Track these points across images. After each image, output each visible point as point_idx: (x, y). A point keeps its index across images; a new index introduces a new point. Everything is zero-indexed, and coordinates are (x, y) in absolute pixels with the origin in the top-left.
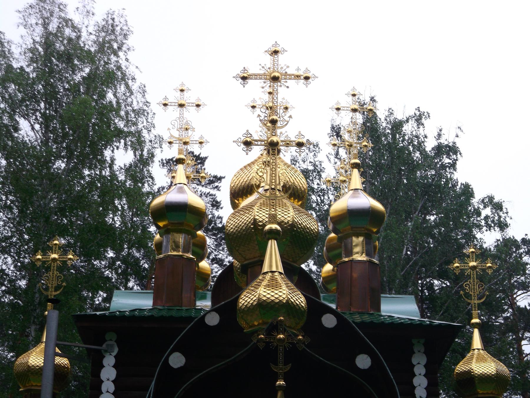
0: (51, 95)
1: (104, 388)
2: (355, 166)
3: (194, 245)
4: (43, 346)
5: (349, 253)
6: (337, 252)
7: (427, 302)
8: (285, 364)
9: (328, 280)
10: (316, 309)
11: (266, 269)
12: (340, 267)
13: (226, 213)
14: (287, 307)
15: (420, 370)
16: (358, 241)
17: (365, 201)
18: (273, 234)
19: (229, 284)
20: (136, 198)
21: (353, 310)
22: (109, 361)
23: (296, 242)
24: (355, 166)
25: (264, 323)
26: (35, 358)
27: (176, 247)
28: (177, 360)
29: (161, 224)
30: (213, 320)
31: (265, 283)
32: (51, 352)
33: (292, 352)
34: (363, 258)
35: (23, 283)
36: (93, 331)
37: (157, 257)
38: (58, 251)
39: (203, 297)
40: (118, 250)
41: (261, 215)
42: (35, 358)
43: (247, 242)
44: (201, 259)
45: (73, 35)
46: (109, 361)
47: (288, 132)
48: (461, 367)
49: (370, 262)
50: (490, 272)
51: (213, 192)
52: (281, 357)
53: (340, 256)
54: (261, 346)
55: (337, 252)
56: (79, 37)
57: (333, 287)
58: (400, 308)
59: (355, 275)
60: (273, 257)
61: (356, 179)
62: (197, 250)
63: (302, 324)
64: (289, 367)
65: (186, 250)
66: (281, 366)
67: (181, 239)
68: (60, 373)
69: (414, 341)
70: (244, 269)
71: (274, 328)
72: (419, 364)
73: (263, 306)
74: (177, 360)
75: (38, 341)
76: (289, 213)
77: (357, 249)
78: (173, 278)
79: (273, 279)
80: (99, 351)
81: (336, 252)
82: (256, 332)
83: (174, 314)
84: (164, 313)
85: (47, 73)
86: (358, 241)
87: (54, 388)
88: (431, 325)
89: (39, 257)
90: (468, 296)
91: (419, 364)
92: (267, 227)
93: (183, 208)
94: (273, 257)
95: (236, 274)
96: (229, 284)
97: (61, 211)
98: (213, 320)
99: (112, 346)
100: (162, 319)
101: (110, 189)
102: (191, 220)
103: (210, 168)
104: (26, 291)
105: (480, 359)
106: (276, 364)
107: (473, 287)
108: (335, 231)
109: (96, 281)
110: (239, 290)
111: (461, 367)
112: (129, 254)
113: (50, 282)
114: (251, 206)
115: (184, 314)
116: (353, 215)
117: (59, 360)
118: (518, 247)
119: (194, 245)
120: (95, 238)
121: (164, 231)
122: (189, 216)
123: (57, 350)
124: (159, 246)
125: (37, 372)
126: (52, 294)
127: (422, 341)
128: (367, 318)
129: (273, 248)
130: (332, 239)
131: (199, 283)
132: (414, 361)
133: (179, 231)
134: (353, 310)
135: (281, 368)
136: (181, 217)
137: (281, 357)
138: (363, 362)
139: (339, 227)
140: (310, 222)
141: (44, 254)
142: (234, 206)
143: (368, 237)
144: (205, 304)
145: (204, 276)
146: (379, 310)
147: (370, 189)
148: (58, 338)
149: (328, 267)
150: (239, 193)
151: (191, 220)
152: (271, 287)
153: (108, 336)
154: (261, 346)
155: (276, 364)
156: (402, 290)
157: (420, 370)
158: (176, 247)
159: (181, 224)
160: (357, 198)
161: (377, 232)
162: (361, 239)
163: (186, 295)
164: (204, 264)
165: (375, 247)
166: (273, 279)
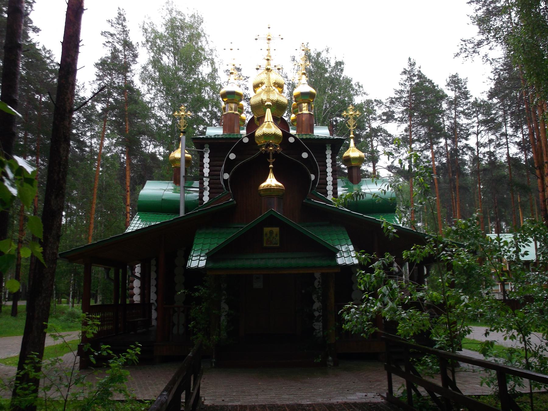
0: (175, 46)
1: (205, 166)
2: (304, 74)
3: (239, 108)
4: (180, 149)
5: (301, 110)
6: (296, 109)
7: (332, 128)
8: (273, 159)
9: (293, 121)
10: (286, 135)
11: (266, 120)
12: (298, 116)
13: (251, 93)
14: (275, 135)
15: (329, 156)
16: (305, 105)
17: (308, 89)
18: (269, 106)
19: (253, 125)
20: (214, 88)
21: (303, 133)
22: (206, 155)
23: (278, 108)
24: (304, 74)
25: (266, 142)
26: (177, 154)
27: (231, 109)
28: (232, 156)
29: (225, 100)
30: (246, 140)
31: (266, 126)
32: (183, 152)
33: (276, 155)
34: (307, 112)
35: (170, 123)
36: (200, 143)
37: (224, 113)
38: (184, 112)
39: (243, 129)
40: (207, 108)
41: (264, 97)
42: (177, 154)
43: (259, 108)
44: (242, 113)
45: (182, 18)
46: (206, 155)
47: (272, 63)
48: (346, 154)
49: (310, 114)
50: (358, 116)
51: (245, 83)
52: (271, 156)
53: (297, 111)
54: (264, 152)
55: (296, 109)
56: (184, 19)
57: (295, 123)
58: (321, 132)
59: (304, 119)
60: (269, 115)
61: (304, 79)
62: (240, 110)
63: (280, 142)
64: (274, 160)
65: (235, 111)
66: (271, 159)
67: (233, 106)
68: (187, 161)
69: (327, 145)
70: (258, 119)
71: (268, 145)
72: (329, 153)
73: (265, 135)
74: (232, 156)
75: (178, 148)
76: (276, 96)
77: (304, 109)
78: (230, 122)
79: (269, 124)
80: (202, 152)
81: (296, 110)
82: (261, 146)
83: (231, 136)
84: (227, 136)
85: (174, 36)
86: (305, 105)
87: (186, 166)
88: (333, 139)
89: (176, 114)
90: (349, 126)
91: (329, 153)
92: (266, 104)
93: (233, 93)
94: (269, 115)
95: (256, 120)
96: (253, 125)
97: (183, 92)
98: (246, 140)
99: (207, 150)
100: (226, 139)
101: (202, 84)
102: (237, 98)
103: (244, 73)
104: (171, 126)
105: (353, 151)
106: (269, 159)
107: (351, 123)
108: (296, 101)
109: (200, 121)
110: (257, 127)
111: (346, 154)
112: (212, 110)
113: (182, 123)
114: (260, 94)
115: (236, 137)
116: (303, 94)
117: (186, 155)
118: (373, 103)
119: (239, 108)
120: (199, 103)
121: (227, 103)
122: (236, 96)
123: (186, 151)
124: (224, 108)
125: (179, 160)
126: (182, 129)
127: (330, 145)
128: (308, 137)
129: (268, 112)
130: (294, 105)
131: (241, 123)
132: (327, 153)
133: (232, 103)
134: (303, 133)
135: (271, 160)
136: (233, 97)
137: (271, 156)
138: (305, 155)
139: (297, 100)
140: (284, 99)
141: (178, 112)
142: (255, 91)
143: (309, 103)
144: (244, 132)
145: (243, 121)
146: (313, 133)
147: (310, 84)
148: (186, 146)
149: (293, 116)
150: (256, 86)
151: (237, 98)
152: (269, 127)
153: (205, 146)
154: (264, 152)
155: (269, 159)
156: (323, 124)
157: (329, 156)
158: (231, 109)
159: (233, 100)
160: (304, 87)
161: (313, 101)
162: (306, 104)
163: (236, 128)
164: (243, 116)
165: (312, 107)
166: (269, 124)
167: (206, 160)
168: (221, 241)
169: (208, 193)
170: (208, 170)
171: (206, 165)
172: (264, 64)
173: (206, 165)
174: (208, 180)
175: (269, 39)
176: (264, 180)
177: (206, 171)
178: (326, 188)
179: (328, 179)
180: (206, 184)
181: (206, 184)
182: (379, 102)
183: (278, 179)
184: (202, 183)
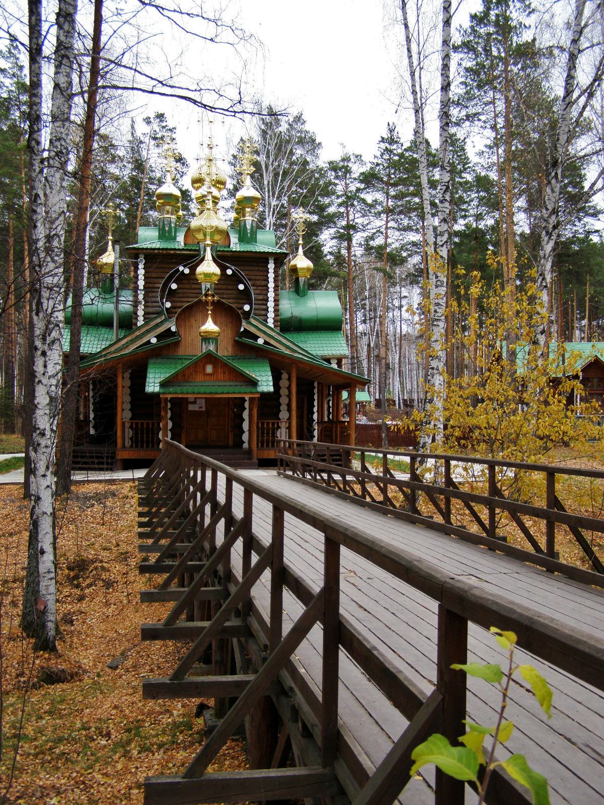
1: (139, 278)
22: (141, 266)
46: (141, 266)
48: (292, 263)
72: (271, 266)
77: (247, 215)
91: (271, 266)
162: (254, 169)
167: (141, 272)
168: (168, 375)
169: (143, 307)
170: (143, 283)
171: (141, 277)
172: (206, 142)
173: (141, 277)
174: (143, 292)
175: (210, 160)
176: (204, 323)
177: (141, 283)
178: (266, 305)
179: (269, 295)
180: (141, 297)
181: (141, 297)
182: (358, 157)
183: (215, 323)
184: (136, 296)
